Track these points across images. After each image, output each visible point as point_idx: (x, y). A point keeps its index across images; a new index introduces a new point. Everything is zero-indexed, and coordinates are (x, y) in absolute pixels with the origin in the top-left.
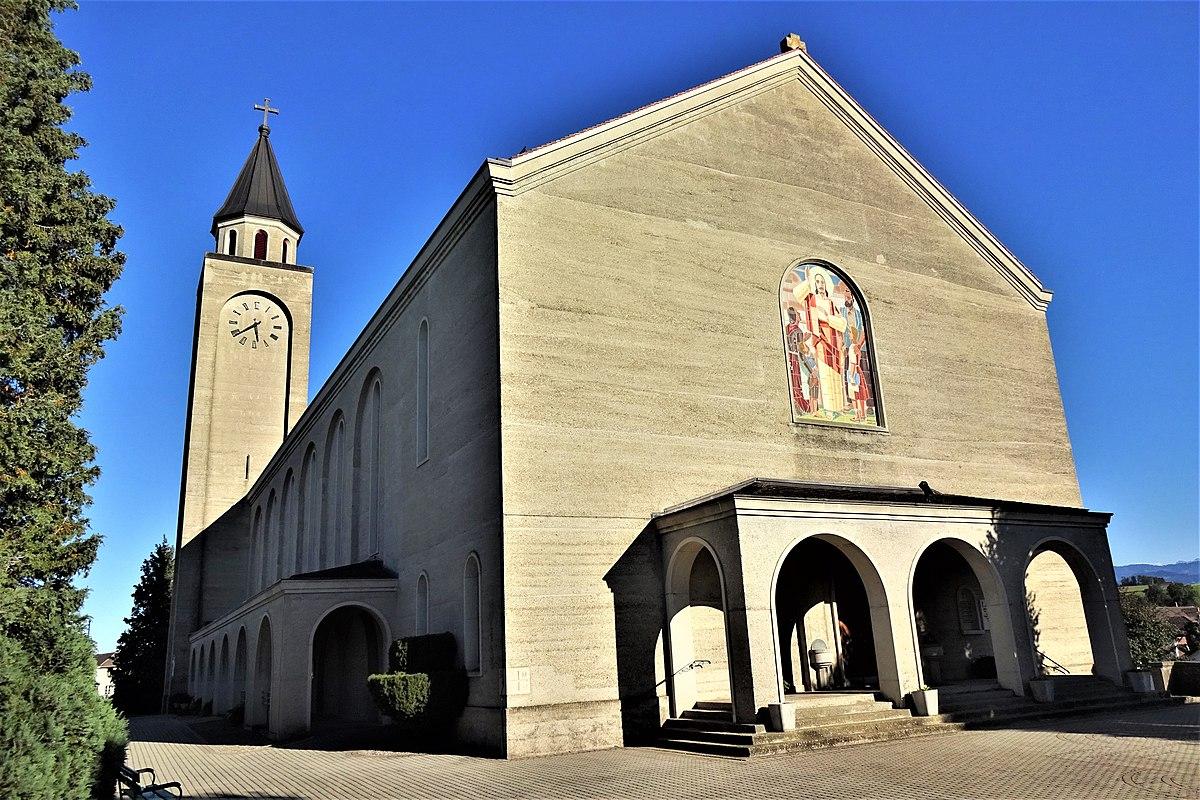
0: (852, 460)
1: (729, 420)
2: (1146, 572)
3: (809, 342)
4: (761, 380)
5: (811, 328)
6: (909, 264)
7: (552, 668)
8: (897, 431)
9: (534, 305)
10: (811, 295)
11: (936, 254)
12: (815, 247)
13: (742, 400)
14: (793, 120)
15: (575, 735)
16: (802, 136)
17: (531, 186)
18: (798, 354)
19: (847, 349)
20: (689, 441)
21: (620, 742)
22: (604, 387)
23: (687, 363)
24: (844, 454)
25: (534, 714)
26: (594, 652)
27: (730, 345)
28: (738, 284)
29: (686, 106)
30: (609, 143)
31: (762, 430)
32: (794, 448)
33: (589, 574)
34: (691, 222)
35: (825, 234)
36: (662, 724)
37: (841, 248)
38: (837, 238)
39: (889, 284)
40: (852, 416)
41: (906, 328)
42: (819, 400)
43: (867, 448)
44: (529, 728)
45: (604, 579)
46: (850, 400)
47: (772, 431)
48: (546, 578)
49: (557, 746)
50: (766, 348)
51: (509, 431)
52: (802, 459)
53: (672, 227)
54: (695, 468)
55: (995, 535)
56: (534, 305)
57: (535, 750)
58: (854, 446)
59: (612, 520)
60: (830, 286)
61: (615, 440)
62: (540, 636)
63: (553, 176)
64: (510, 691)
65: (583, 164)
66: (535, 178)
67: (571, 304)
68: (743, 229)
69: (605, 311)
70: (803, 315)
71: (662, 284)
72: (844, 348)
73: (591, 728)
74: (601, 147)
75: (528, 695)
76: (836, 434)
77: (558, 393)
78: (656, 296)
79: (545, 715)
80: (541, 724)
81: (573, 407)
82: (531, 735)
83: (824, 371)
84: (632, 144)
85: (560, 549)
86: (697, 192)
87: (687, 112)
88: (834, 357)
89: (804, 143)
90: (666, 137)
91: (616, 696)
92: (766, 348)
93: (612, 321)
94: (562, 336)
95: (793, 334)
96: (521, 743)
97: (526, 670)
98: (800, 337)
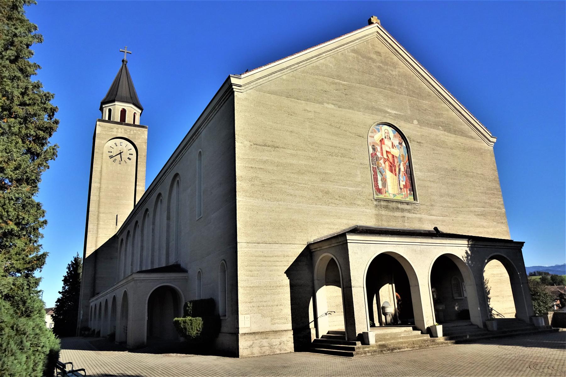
8: (423, 203)
10: (383, 139)
13: (350, 189)
18: (376, 167)
19: (400, 165)
28: (348, 134)
46: (401, 189)
50: (361, 164)
72: (398, 164)
88: (393, 168)
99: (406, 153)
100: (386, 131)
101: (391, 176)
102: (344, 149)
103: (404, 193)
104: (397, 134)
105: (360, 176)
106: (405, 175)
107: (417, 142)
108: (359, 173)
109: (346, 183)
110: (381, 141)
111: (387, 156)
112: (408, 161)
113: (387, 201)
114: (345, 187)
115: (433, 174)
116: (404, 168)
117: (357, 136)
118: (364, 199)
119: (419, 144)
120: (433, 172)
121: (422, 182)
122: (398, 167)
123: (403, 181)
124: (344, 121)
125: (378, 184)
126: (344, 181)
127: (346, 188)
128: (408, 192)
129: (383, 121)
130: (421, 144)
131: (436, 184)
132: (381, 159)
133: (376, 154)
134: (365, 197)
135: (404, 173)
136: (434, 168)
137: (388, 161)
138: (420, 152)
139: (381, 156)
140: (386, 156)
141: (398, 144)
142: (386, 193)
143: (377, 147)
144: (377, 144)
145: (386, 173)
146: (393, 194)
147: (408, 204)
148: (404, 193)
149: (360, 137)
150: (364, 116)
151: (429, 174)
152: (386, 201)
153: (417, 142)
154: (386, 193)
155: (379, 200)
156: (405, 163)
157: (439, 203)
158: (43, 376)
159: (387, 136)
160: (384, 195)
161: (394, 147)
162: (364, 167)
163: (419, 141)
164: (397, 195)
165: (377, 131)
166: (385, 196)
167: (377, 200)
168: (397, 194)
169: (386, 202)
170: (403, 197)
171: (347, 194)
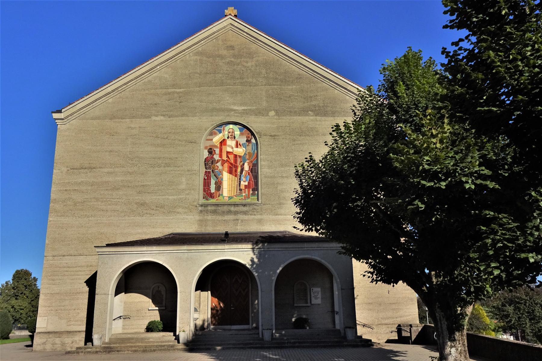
0: (234, 220)
1: (162, 207)
2: (194, 301)
3: (219, 164)
4: (183, 187)
5: (221, 156)
6: (292, 112)
7: (57, 317)
9: (69, 169)
10: (224, 140)
11: (314, 103)
12: (228, 115)
13: (170, 197)
14: (224, 52)
15: (63, 344)
16: (228, 60)
17: (73, 118)
19: (244, 164)
20: (138, 219)
22: (97, 200)
23: (142, 184)
24: (231, 217)
25: (46, 335)
26: (77, 311)
27: (168, 172)
28: (176, 142)
29: (156, 63)
30: (113, 91)
31: (180, 210)
32: (197, 217)
33: (79, 279)
34: (154, 118)
35: (236, 108)
37: (245, 113)
38: (243, 108)
39: (275, 126)
40: (241, 198)
41: (283, 148)
42: (220, 192)
43: (245, 213)
44: (44, 340)
45: (85, 282)
46: (241, 190)
47: (186, 210)
48: (60, 281)
49: (54, 348)
51: (51, 223)
52: (201, 222)
53: (143, 122)
54: (139, 231)
55: (256, 260)
56: (69, 169)
57: (45, 349)
58: (236, 213)
59: (94, 256)
60: (237, 133)
61: (100, 222)
62: (53, 304)
63: (84, 112)
64: (38, 326)
65: (99, 103)
66: (75, 114)
67: (87, 165)
68: (183, 115)
69: (103, 166)
70: (217, 151)
71: (134, 149)
73: (71, 342)
74: (109, 93)
75: (46, 327)
76: (226, 208)
77: (75, 204)
78: (130, 156)
79: (51, 336)
80: (49, 339)
81: (82, 210)
82: (44, 343)
83: (226, 176)
84: (127, 88)
85: (67, 269)
86: (160, 102)
87: (157, 65)
88: (234, 169)
89: (229, 63)
90: (146, 80)
91: (84, 329)
93: (106, 170)
94: (80, 180)
95: (209, 163)
96: (39, 346)
97: (46, 318)
98: (214, 162)
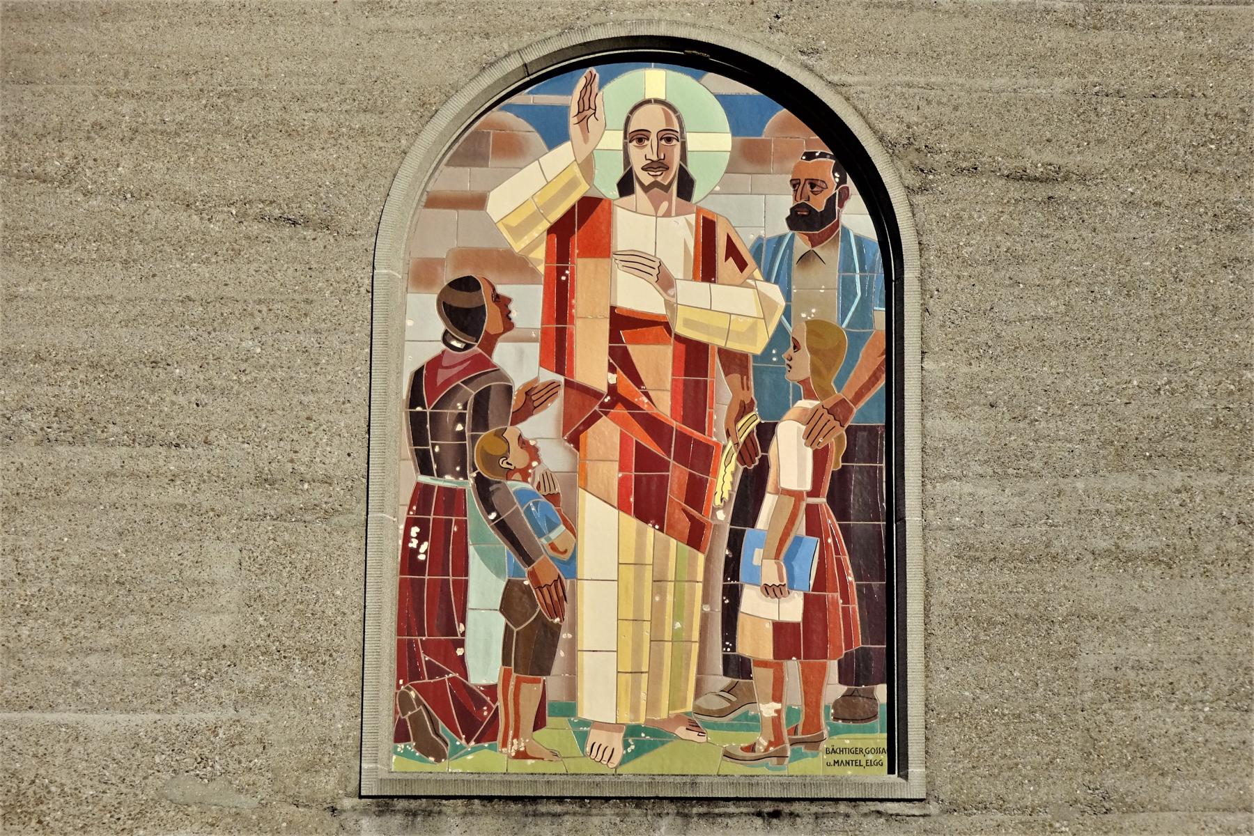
8: (986, 790)
10: (589, 205)
13: (98, 722)
18: (469, 484)
19: (766, 433)
21: (618, 196)
27: (74, 491)
28: (158, 216)
36: (438, 384)
42: (554, 684)
46: (738, 667)
50: (264, 481)
72: (750, 423)
88: (677, 475)
92: (264, 481)
99: (865, 305)
100: (651, 120)
101: (640, 547)
102: (93, 366)
103: (768, 709)
104: (783, 127)
105: (229, 596)
106: (814, 527)
107: (1020, 177)
108: (224, 571)
109: (61, 673)
110: (562, 231)
111: (621, 360)
112: (882, 383)
113: (513, 807)
114: (52, 707)
115: (1178, 479)
116: (820, 458)
117: (256, 228)
118: (247, 803)
119: (1042, 191)
120: (1185, 459)
121: (1007, 577)
122: (745, 454)
123: (770, 591)
124: (125, 109)
125: (461, 644)
126: (44, 663)
127: (51, 717)
128: (834, 690)
129: (593, 35)
130: (1060, 190)
131: (1199, 582)
132: (532, 401)
133: (482, 364)
134: (263, 781)
135: (812, 511)
136: (1196, 417)
137: (620, 410)
138: (1031, 274)
139: (549, 376)
140: (602, 356)
141: (784, 228)
142: (539, 723)
143: (501, 290)
144: (517, 266)
145: (572, 528)
146: (633, 731)
147: (776, 814)
148: (768, 709)
149: (287, 231)
150: (374, 23)
151: (1128, 482)
152: (498, 806)
153: (1020, 177)
154: (539, 723)
155: (414, 804)
156: (839, 411)
157: (1212, 775)
158: (489, 192)
159: (658, 165)
160: (515, 746)
161: (726, 267)
162: (297, 502)
163: (1036, 159)
164: (681, 731)
165: (536, 139)
166: (521, 755)
167: (402, 804)
168: (679, 719)
169: (507, 815)
170: (751, 748)
171: (62, 777)
